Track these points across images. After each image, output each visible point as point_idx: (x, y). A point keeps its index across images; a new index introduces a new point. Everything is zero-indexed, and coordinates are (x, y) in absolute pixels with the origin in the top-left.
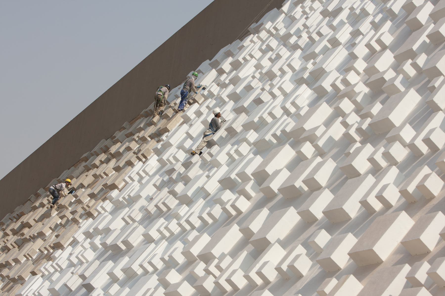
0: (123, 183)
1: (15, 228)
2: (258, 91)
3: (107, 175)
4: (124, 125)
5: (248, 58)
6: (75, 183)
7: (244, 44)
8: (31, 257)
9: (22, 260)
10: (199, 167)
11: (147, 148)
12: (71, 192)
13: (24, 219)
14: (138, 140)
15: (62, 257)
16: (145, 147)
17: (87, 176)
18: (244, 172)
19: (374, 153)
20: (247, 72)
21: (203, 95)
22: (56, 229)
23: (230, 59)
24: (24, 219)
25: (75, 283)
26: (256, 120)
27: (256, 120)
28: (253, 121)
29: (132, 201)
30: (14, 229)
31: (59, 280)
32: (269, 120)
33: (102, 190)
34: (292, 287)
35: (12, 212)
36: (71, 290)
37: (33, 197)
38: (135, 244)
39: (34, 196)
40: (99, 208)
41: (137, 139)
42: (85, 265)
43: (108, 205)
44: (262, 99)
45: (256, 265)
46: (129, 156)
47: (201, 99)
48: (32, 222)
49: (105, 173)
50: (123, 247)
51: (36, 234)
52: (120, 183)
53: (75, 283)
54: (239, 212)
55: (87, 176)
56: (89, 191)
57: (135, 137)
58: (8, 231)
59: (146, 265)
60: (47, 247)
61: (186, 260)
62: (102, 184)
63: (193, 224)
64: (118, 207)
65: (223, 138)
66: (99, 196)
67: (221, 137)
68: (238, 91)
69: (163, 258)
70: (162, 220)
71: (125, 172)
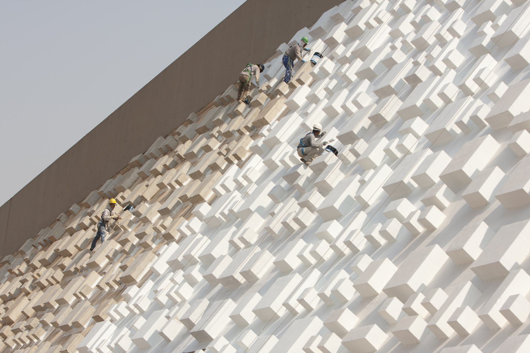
0: (211, 194)
1: (47, 258)
3: (180, 184)
4: (189, 117)
6: (129, 196)
7: (361, 5)
8: (85, 296)
9: (70, 300)
10: (340, 169)
11: (239, 146)
12: (128, 208)
13: (60, 245)
14: (218, 136)
15: (140, 295)
16: (234, 146)
17: (147, 186)
18: (425, 174)
19: (389, 145)
20: (376, 41)
21: (312, 74)
23: (343, 26)
24: (59, 246)
25: (174, 330)
26: (419, 103)
27: (419, 103)
28: (415, 105)
29: (238, 218)
30: (45, 259)
31: (146, 328)
32: (439, 103)
33: (178, 203)
35: (34, 237)
36: (167, 340)
37: (63, 216)
38: (260, 276)
39: (65, 215)
40: (183, 229)
41: (217, 135)
42: (187, 307)
43: (196, 224)
45: (496, 300)
47: (308, 78)
48: (72, 250)
49: (177, 182)
50: (242, 280)
51: (85, 266)
52: (207, 193)
53: (174, 330)
54: (303, 226)
55: (147, 186)
56: (158, 206)
57: (215, 132)
58: (36, 262)
61: (358, 294)
62: (179, 196)
64: (213, 227)
65: (366, 129)
66: (174, 212)
67: (363, 128)
68: (372, 67)
70: (301, 244)
71: (213, 179)
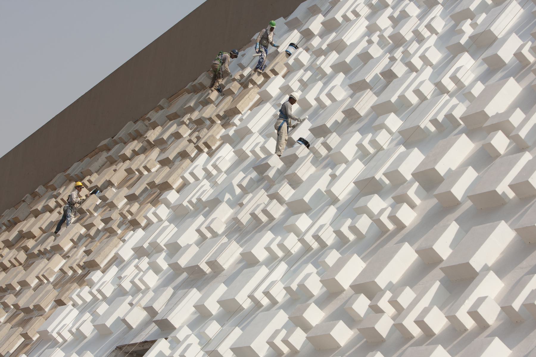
0: (180, 181)
1: (11, 239)
2: (386, 61)
3: (148, 170)
5: (351, 16)
6: (96, 179)
8: (47, 280)
9: (33, 282)
10: (311, 162)
11: (210, 134)
12: (95, 192)
13: (24, 226)
14: (189, 123)
15: (103, 281)
17: (115, 170)
20: (353, 35)
21: (287, 65)
22: (80, 241)
23: (320, 18)
28: (390, 101)
30: (8, 240)
32: (414, 100)
34: (532, 334)
36: (130, 327)
40: (150, 215)
41: (188, 122)
42: (151, 294)
44: (393, 71)
46: (181, 145)
49: (146, 168)
51: (49, 248)
52: (175, 181)
54: (271, 218)
56: (125, 191)
57: (186, 119)
59: (259, 295)
60: (75, 266)
61: (325, 289)
62: (146, 182)
63: (325, 240)
67: (336, 122)
68: (348, 60)
69: (290, 287)
